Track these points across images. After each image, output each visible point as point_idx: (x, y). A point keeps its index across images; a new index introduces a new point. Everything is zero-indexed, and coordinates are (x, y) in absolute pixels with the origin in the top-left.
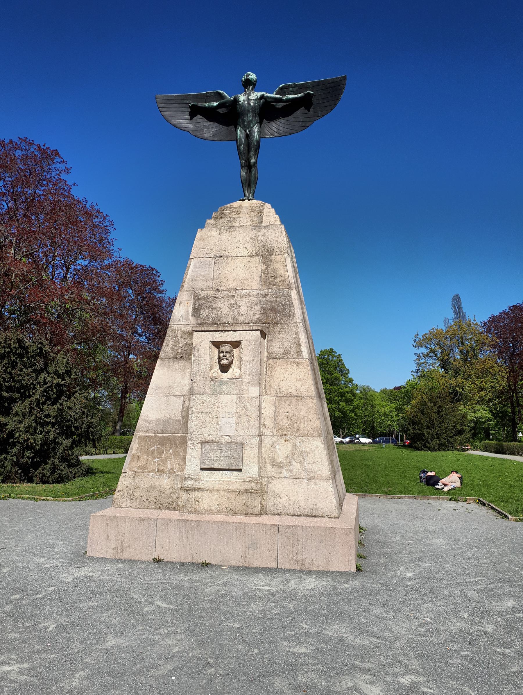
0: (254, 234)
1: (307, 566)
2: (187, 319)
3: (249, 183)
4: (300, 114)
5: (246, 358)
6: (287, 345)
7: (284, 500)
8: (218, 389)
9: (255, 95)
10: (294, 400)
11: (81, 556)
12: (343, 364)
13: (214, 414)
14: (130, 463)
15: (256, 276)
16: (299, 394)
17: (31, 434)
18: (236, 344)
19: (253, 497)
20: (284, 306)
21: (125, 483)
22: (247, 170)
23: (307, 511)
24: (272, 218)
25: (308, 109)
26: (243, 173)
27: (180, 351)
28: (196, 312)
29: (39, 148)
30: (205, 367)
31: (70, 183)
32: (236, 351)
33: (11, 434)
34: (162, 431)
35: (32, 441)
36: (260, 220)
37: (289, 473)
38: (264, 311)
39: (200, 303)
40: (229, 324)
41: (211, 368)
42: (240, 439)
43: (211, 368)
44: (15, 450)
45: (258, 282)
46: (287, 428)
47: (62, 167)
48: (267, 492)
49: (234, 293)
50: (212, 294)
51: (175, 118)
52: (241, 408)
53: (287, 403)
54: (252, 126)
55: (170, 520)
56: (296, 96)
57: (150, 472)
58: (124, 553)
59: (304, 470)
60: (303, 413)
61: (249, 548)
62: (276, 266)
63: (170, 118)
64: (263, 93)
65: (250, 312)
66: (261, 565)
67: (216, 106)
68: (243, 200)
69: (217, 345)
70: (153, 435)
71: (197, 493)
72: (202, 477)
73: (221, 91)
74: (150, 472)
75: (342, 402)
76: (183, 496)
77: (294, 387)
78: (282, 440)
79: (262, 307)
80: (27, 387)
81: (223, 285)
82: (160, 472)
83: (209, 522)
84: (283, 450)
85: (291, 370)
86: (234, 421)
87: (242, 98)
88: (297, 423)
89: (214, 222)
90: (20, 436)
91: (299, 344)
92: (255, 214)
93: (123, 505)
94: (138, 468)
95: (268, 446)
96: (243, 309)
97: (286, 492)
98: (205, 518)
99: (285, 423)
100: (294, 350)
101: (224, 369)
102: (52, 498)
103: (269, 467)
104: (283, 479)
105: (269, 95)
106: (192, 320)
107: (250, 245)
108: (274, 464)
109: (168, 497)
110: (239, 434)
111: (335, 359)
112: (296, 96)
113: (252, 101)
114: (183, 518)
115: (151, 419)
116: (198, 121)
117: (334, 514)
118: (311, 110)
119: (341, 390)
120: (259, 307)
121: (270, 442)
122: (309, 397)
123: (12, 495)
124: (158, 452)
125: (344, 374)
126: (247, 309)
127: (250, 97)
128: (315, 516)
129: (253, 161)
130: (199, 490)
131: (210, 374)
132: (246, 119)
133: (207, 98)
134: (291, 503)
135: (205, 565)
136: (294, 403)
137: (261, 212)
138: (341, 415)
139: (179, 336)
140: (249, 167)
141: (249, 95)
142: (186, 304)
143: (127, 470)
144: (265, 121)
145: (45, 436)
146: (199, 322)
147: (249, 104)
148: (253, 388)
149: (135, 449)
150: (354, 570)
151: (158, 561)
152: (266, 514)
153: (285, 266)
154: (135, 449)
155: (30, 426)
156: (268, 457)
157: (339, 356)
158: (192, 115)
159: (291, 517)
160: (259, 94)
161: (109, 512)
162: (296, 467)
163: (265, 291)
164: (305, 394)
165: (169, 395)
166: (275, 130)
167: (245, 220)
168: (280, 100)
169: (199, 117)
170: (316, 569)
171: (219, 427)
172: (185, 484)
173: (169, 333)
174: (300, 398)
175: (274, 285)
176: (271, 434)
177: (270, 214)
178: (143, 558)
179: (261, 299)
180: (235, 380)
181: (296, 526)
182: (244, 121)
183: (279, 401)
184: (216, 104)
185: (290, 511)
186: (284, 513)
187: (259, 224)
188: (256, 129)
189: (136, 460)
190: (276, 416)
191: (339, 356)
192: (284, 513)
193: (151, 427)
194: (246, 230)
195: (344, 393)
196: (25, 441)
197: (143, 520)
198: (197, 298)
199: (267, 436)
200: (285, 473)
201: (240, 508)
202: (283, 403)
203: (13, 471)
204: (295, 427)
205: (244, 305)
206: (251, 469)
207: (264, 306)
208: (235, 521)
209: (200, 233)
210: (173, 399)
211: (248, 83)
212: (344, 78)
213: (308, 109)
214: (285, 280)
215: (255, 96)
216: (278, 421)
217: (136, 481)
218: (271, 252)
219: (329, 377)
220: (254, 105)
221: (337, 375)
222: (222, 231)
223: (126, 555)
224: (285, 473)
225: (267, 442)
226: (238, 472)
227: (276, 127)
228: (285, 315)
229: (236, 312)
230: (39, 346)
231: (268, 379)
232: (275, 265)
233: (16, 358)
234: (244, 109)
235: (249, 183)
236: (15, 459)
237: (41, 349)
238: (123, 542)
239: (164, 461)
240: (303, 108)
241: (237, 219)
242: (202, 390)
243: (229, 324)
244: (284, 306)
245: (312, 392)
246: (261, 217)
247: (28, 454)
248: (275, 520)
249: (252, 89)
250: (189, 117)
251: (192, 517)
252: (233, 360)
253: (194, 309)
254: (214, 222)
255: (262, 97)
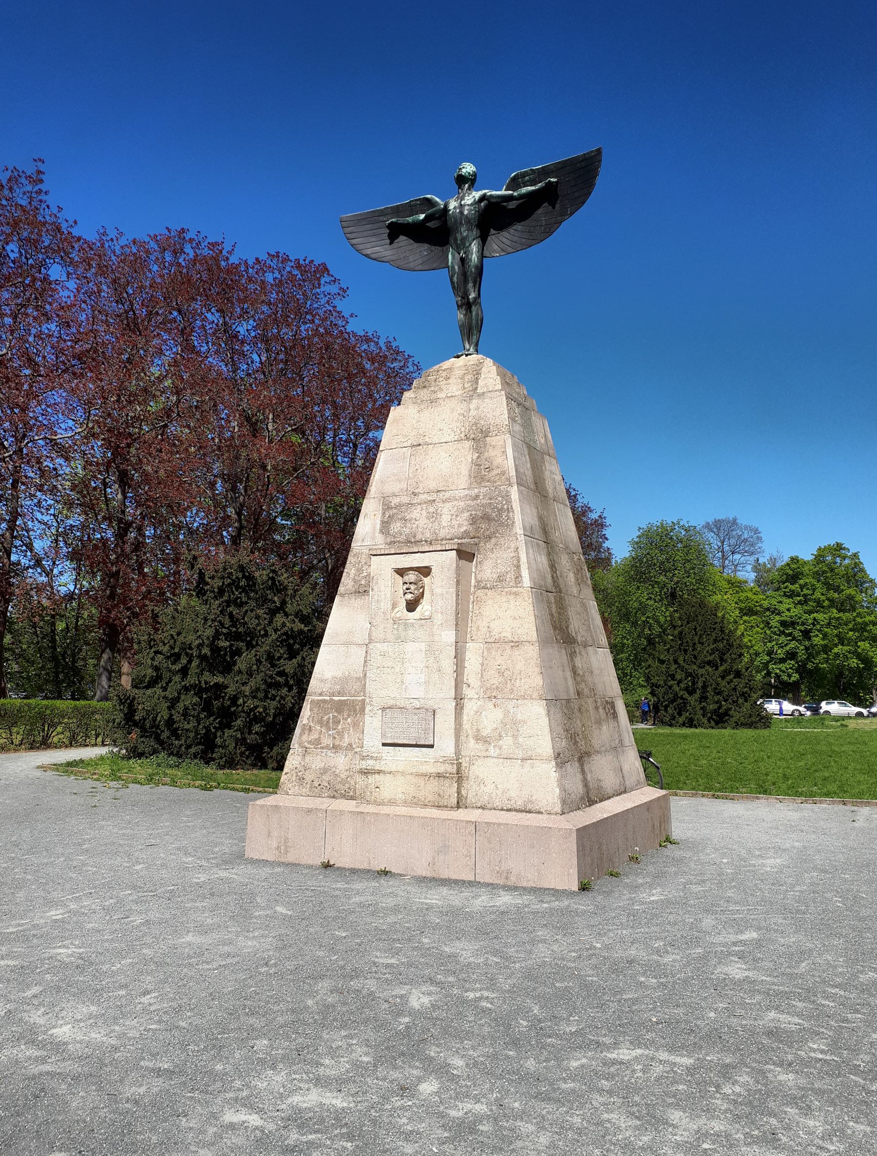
0: (465, 409)
1: (513, 880)
2: (373, 538)
3: (470, 329)
4: (542, 213)
5: (438, 591)
6: (501, 569)
7: (489, 788)
8: (403, 634)
9: (471, 196)
10: (508, 647)
11: (240, 857)
12: (862, 570)
13: (397, 669)
14: (301, 735)
15: (465, 471)
16: (516, 639)
17: (261, 700)
18: (425, 571)
19: (447, 782)
20: (500, 511)
21: (294, 762)
22: (466, 310)
23: (519, 804)
24: (491, 380)
25: (553, 205)
26: (460, 316)
27: (363, 583)
28: (385, 526)
29: (298, 266)
30: (386, 605)
31: (346, 314)
32: (426, 580)
33: (234, 699)
34: (339, 694)
35: (261, 710)
36: (474, 386)
37: (498, 751)
38: (473, 521)
39: (391, 514)
40: (426, 541)
41: (394, 606)
42: (431, 704)
43: (394, 606)
44: (239, 722)
45: (466, 478)
46: (497, 688)
47: (334, 289)
48: (468, 777)
49: (434, 496)
50: (405, 500)
51: (369, 245)
52: (431, 660)
53: (499, 652)
54: (467, 244)
55: (342, 813)
56: (533, 188)
57: (322, 748)
58: (289, 854)
59: (518, 745)
60: (520, 666)
61: (439, 852)
62: (491, 453)
63: (360, 247)
64: (484, 191)
65: (454, 522)
66: (454, 877)
67: (423, 220)
68: (458, 357)
69: (401, 572)
70: (328, 698)
71: (377, 776)
72: (384, 755)
73: (429, 196)
74: (322, 748)
75: (864, 641)
76: (360, 780)
77: (509, 629)
78: (490, 705)
79: (471, 515)
80: (251, 634)
81: (421, 485)
82: (336, 748)
83: (389, 815)
84: (490, 719)
85: (506, 604)
86: (423, 678)
87: (453, 205)
88: (510, 680)
89: (413, 396)
90: (244, 703)
91: (518, 567)
92: (470, 376)
93: (290, 792)
94: (310, 742)
95: (472, 713)
96: (445, 519)
97: (491, 778)
98: (385, 810)
99: (495, 680)
100: (510, 576)
101: (411, 606)
102: (271, 790)
103: (472, 742)
104: (489, 759)
105: (494, 193)
106: (380, 539)
107: (458, 424)
108: (478, 738)
109: (343, 782)
110: (430, 696)
111: (847, 561)
112: (533, 188)
113: (467, 208)
114: (358, 810)
115: (326, 677)
116: (401, 244)
117: (555, 810)
118: (557, 206)
119: (859, 620)
120: (467, 514)
121: (475, 708)
122: (529, 642)
123: (222, 785)
124: (334, 722)
125: (864, 590)
126: (452, 521)
127: (463, 203)
128: (530, 812)
129: (472, 296)
130: (379, 772)
131: (393, 615)
132: (459, 237)
133: (412, 208)
134: (499, 792)
135: (385, 873)
136: (508, 652)
137: (478, 373)
138: (862, 666)
139: (363, 561)
140: (467, 305)
141: (462, 199)
142: (372, 517)
143: (296, 746)
144: (492, 231)
145: (279, 702)
146: (389, 540)
147: (461, 213)
148: (447, 632)
149: (306, 717)
150: (575, 888)
151: (327, 866)
152: (466, 807)
153: (504, 452)
154: (306, 717)
155: (258, 689)
156: (472, 728)
157: (855, 555)
158: (392, 237)
159: (497, 812)
160: (477, 195)
161: (271, 800)
162: (507, 742)
163: (476, 491)
164: (524, 638)
165: (347, 644)
166: (508, 243)
167: (454, 387)
168: (510, 198)
169: (402, 238)
170: (524, 884)
171: (404, 687)
172: (364, 765)
173: (351, 559)
174: (516, 644)
175: (488, 481)
176: (476, 696)
177: (490, 374)
178: (310, 862)
179: (470, 502)
180: (423, 621)
181: (499, 824)
182: (456, 239)
183: (489, 649)
184: (422, 216)
185: (498, 804)
186: (489, 806)
187: (473, 392)
188: (474, 247)
189: (307, 732)
190: (483, 670)
191: (855, 555)
192: (489, 806)
193: (326, 688)
194: (453, 403)
195: (866, 624)
196: (251, 710)
197: (309, 811)
198: (387, 507)
199: (471, 699)
200: (492, 751)
201: (430, 797)
202: (493, 653)
203: (238, 751)
204: (508, 686)
205: (446, 511)
206: (446, 746)
207: (473, 512)
208: (422, 815)
209: (395, 412)
210: (353, 649)
211: (461, 180)
212: (599, 151)
213: (553, 205)
214: (503, 473)
215: (472, 197)
216: (485, 678)
217: (307, 760)
218: (486, 433)
219: (836, 595)
220: (469, 213)
221: (852, 591)
222: (422, 407)
223: (290, 858)
224: (492, 751)
225: (470, 707)
226: (429, 749)
227: (498, 241)
228: (502, 524)
229: (436, 523)
230: (271, 575)
231: (474, 619)
232: (490, 451)
233: (240, 593)
234: (456, 220)
235: (470, 329)
236: (239, 736)
237: (273, 579)
238: (286, 840)
239: (341, 734)
240: (546, 204)
241: (444, 388)
242: (382, 636)
243: (426, 541)
244: (500, 511)
245: (533, 635)
246: (477, 383)
247: (257, 728)
248: (474, 815)
249: (469, 189)
250: (388, 241)
251: (371, 809)
252: (423, 593)
253: (383, 522)
254: (413, 396)
255: (483, 198)
